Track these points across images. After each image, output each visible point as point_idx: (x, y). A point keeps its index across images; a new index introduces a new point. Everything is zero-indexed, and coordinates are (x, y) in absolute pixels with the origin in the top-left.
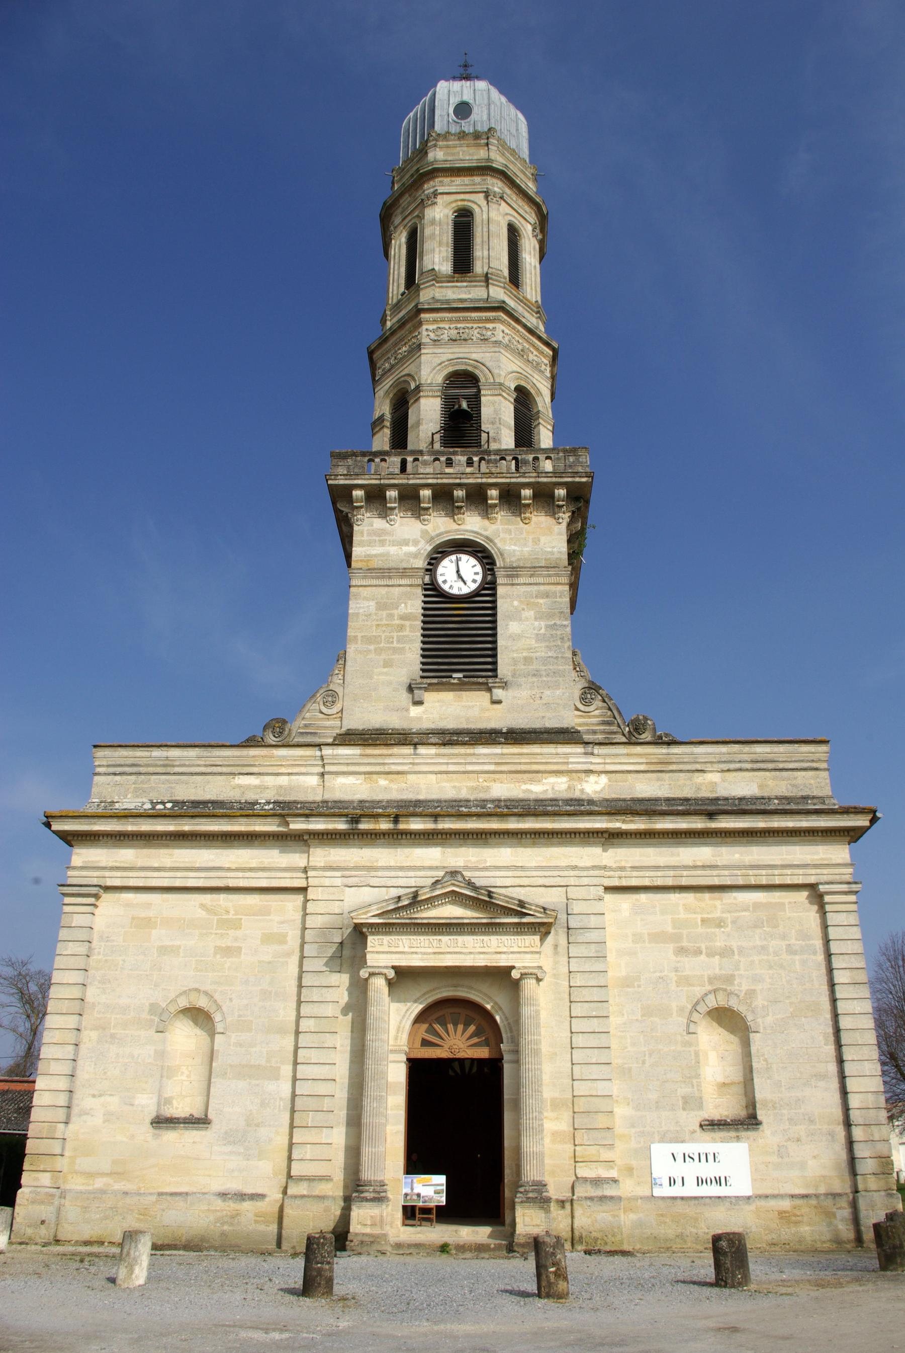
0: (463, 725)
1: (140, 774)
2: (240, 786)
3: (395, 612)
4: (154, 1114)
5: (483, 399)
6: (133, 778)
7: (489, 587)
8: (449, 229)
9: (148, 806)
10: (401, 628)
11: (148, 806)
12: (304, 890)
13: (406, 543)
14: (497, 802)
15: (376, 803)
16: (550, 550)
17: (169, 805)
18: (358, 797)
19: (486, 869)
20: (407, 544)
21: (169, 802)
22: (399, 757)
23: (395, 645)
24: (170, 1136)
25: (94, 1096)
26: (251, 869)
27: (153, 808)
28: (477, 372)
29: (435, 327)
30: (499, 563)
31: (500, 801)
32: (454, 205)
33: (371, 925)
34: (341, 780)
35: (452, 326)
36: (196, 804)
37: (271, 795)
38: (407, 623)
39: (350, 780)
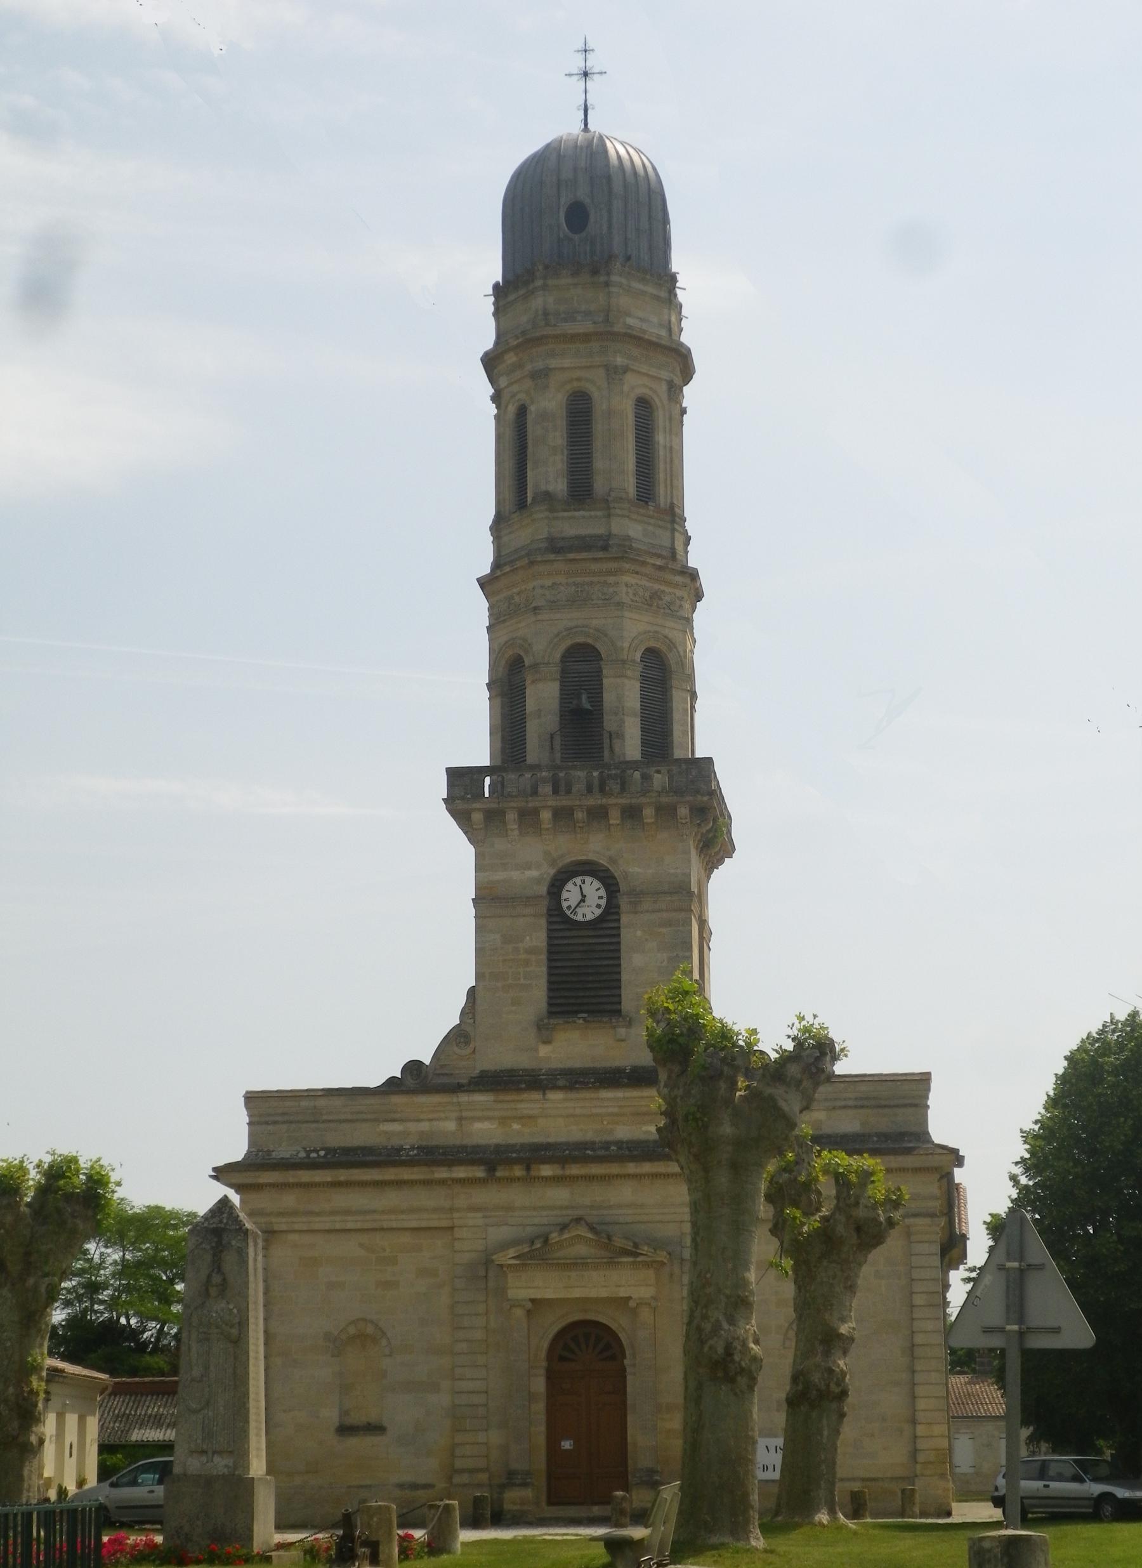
0: (588, 1064)
1: (291, 1122)
2: (386, 1133)
3: (520, 945)
4: (337, 1424)
5: (605, 681)
6: (285, 1126)
7: (611, 911)
8: (562, 423)
9: (302, 1154)
10: (527, 963)
11: (302, 1154)
12: (452, 1228)
13: (528, 866)
14: (619, 1144)
15: (510, 1148)
16: (672, 871)
17: (322, 1153)
18: (495, 1141)
19: (610, 1207)
20: (530, 868)
21: (322, 1149)
22: (529, 1102)
23: (522, 981)
24: (353, 1442)
25: (284, 1411)
26: (402, 1212)
27: (308, 1156)
28: (598, 646)
29: (548, 583)
30: (623, 887)
31: (622, 1142)
32: (568, 387)
33: (510, 1266)
34: (478, 1125)
35: (571, 580)
36: (347, 1151)
37: (413, 1140)
38: (533, 958)
39: (486, 1125)
